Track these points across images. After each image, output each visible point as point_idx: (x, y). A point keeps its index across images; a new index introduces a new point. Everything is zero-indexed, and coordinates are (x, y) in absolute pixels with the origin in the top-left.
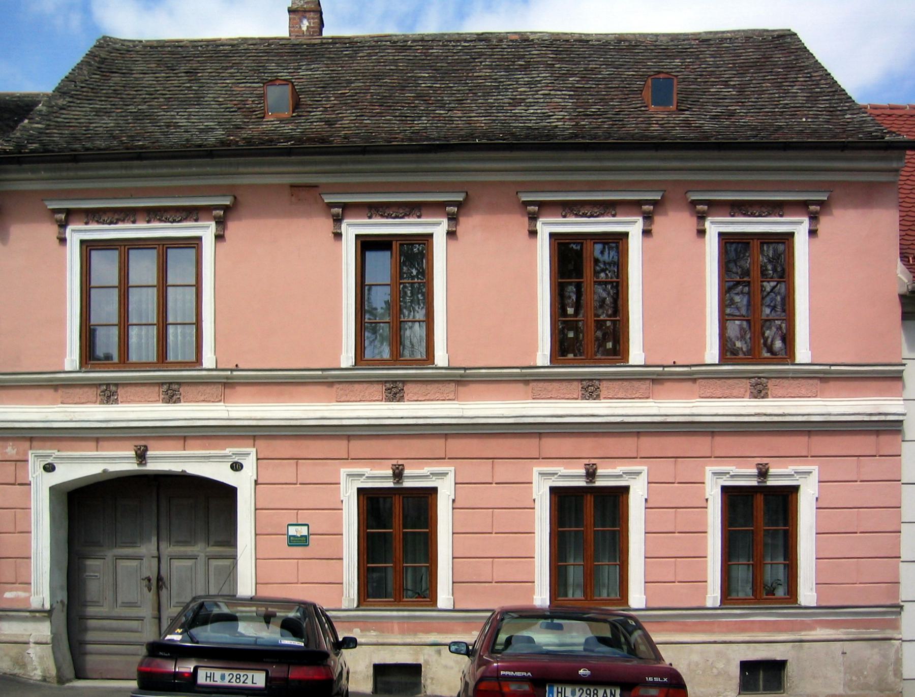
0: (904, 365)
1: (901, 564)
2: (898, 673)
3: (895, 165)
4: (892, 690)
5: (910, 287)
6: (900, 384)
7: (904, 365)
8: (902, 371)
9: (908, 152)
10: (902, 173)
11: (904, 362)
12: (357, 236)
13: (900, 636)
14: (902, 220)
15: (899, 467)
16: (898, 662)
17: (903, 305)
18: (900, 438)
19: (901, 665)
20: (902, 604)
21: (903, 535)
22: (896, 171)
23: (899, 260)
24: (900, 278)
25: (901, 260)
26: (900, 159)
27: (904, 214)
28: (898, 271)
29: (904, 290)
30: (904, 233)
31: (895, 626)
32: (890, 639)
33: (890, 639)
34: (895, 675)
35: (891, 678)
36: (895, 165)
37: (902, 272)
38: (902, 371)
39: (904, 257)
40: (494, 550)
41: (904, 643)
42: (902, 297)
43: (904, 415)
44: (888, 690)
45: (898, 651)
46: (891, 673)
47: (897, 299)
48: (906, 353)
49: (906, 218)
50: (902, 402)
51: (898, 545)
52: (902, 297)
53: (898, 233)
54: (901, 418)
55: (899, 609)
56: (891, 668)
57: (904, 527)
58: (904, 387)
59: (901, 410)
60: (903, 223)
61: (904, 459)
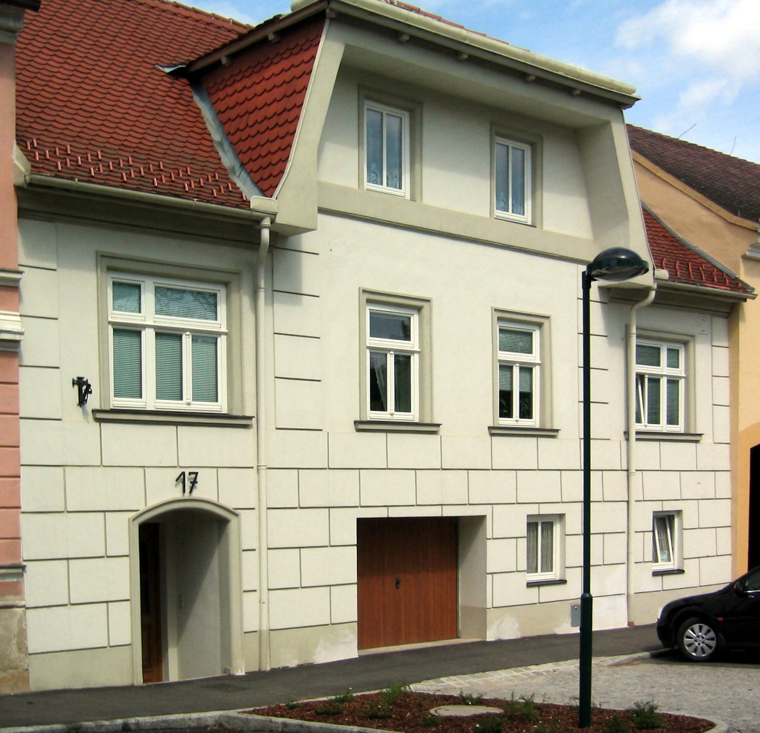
0: (21, 273)
1: (22, 516)
2: (22, 647)
3: (11, 24)
4: (17, 668)
5: (28, 178)
6: (16, 295)
7: (21, 273)
8: (18, 280)
9: (27, 11)
10: (23, 35)
11: (21, 269)
12: (410, 340)
13: (23, 603)
14: (19, 94)
15: (16, 397)
16: (22, 634)
17: (19, 199)
18: (16, 361)
19: (25, 638)
20: (24, 563)
21: (23, 481)
22: (13, 31)
23: (15, 142)
24: (16, 166)
25: (18, 144)
26: (18, 18)
27: (21, 89)
28: (14, 157)
29: (20, 181)
30: (21, 112)
31: (17, 589)
32: (12, 607)
33: (12, 607)
34: (20, 650)
35: (15, 654)
36: (11, 24)
37: (17, 158)
38: (18, 280)
39: (21, 141)
40: (293, 597)
41: (28, 611)
42: (18, 189)
43: (21, 334)
44: (12, 668)
45: (22, 620)
46: (15, 648)
47: (12, 190)
48: (23, 259)
49: (23, 94)
50: (18, 318)
51: (16, 492)
52: (18, 189)
53: (14, 110)
54: (17, 337)
55: (20, 571)
56: (14, 641)
57: (23, 471)
58: (20, 299)
59: (17, 328)
60: (20, 99)
61: (21, 385)
